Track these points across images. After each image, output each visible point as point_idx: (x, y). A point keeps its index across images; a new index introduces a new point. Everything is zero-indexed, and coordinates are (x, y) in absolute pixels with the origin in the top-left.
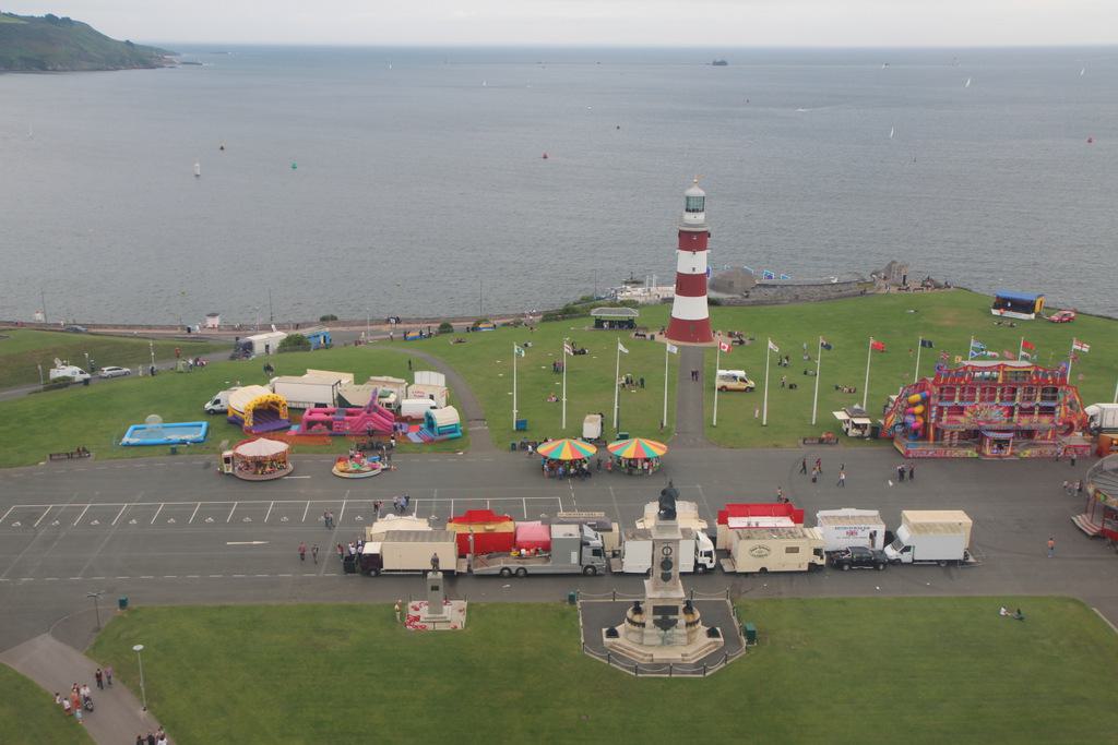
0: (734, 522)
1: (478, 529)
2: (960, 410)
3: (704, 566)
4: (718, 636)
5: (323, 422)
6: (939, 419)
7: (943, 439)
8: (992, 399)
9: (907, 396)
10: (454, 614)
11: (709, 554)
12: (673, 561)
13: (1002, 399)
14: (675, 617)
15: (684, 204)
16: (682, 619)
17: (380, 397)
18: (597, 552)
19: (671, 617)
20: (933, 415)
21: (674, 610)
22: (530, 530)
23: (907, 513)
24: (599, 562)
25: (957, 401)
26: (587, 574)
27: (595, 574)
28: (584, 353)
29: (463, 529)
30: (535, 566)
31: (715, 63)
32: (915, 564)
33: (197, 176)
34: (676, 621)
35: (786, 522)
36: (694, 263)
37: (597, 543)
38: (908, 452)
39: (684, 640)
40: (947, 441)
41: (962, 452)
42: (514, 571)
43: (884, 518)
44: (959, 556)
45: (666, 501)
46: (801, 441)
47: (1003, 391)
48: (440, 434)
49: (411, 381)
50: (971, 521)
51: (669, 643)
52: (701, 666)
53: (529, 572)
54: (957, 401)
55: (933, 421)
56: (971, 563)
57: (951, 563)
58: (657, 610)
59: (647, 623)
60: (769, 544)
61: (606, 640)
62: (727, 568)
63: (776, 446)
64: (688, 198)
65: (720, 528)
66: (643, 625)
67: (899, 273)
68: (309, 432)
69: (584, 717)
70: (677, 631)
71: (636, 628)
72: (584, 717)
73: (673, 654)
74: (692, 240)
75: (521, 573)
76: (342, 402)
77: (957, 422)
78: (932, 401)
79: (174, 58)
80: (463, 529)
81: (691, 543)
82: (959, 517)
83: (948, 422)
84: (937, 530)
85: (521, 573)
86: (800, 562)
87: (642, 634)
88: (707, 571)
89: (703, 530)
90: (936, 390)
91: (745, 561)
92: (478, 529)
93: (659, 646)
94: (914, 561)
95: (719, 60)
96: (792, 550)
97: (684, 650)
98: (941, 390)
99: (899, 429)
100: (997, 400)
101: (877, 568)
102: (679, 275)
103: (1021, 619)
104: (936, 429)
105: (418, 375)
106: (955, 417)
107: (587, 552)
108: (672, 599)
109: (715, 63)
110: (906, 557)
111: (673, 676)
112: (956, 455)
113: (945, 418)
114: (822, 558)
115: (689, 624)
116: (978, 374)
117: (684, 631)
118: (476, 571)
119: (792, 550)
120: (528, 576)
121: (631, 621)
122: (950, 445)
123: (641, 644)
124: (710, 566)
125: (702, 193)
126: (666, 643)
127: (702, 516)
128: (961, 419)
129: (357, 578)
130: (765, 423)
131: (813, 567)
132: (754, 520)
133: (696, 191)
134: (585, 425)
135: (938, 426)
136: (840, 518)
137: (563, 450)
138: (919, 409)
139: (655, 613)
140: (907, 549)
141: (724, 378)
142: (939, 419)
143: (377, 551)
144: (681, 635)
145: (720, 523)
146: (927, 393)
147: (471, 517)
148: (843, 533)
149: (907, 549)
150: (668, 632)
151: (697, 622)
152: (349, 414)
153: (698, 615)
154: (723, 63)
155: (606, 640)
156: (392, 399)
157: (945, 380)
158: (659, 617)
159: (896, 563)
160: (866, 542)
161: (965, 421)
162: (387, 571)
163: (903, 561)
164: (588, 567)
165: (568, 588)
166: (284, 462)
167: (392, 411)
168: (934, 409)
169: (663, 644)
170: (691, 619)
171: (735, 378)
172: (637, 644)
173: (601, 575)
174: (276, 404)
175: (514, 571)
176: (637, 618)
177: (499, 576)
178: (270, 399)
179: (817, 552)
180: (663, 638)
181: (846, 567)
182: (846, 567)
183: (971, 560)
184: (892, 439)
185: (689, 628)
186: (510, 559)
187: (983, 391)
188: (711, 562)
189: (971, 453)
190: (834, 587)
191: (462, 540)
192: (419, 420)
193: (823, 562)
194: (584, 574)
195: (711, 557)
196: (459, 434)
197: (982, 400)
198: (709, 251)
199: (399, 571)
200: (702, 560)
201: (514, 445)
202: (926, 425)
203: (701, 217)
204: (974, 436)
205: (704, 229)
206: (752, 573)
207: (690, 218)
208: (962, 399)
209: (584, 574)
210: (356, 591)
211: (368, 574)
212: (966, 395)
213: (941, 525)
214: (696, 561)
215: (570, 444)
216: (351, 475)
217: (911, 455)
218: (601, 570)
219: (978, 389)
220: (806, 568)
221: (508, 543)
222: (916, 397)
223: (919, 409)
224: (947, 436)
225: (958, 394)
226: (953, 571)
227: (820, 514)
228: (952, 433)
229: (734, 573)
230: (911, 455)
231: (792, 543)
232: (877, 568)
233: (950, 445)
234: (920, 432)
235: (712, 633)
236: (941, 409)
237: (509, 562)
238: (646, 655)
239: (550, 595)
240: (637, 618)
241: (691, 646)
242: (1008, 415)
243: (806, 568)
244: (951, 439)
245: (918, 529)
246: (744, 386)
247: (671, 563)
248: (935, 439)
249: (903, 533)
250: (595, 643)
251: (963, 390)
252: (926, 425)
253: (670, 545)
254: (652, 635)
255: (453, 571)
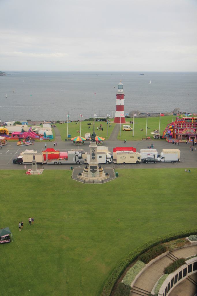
0: (117, 152)
1: (50, 153)
2: (182, 130)
3: (108, 162)
4: (108, 175)
5: (17, 135)
6: (177, 132)
7: (178, 137)
8: (191, 127)
9: (169, 127)
10: (39, 171)
11: (109, 158)
12: (95, 154)
13: (193, 127)
14: (96, 169)
15: (117, 87)
16: (98, 170)
17: (33, 129)
18: (80, 158)
19: (95, 169)
20: (175, 131)
21: (96, 167)
22: (63, 153)
23: (164, 150)
24: (80, 160)
25: (181, 127)
26: (78, 164)
27: (79, 164)
28: (91, 124)
29: (44, 153)
30: (64, 162)
31: (141, 75)
32: (165, 162)
33: (6, 98)
34: (96, 170)
35: (132, 152)
36: (121, 102)
37: (80, 155)
38: (169, 141)
39: (98, 175)
40: (179, 138)
41: (183, 141)
42: (58, 163)
43: (157, 151)
44: (176, 160)
45: (93, 137)
46: (142, 140)
47: (193, 125)
48: (47, 138)
49: (42, 127)
50: (180, 151)
51: (94, 176)
52: (102, 182)
53: (62, 163)
54: (181, 127)
55: (175, 133)
56: (180, 162)
57: (175, 162)
58: (91, 167)
59: (89, 171)
60: (125, 157)
61: (78, 176)
62: (115, 162)
63: (135, 140)
64: (119, 85)
65: (114, 153)
66: (88, 171)
67: (177, 110)
68: (13, 137)
69: (68, 192)
70: (96, 173)
71: (86, 172)
72: (68, 192)
73: (95, 179)
74: (120, 96)
75: (60, 163)
76: (23, 131)
77: (181, 133)
78: (175, 127)
79: (5, 74)
80: (44, 153)
81: (105, 155)
82: (178, 151)
83: (180, 133)
84: (172, 154)
85: (60, 163)
86: (134, 161)
87: (87, 174)
88: (110, 163)
89: (109, 154)
90: (176, 124)
91: (119, 161)
92: (50, 153)
93: (92, 177)
94: (165, 161)
95: (142, 74)
96: (132, 157)
97: (98, 178)
98: (177, 124)
99: (167, 136)
100: (192, 127)
101: (155, 163)
102: (117, 106)
103: (190, 172)
104: (176, 135)
105: (44, 125)
106: (181, 132)
107: (77, 158)
108: (95, 164)
109: (141, 75)
110: (163, 160)
111: (94, 183)
112: (181, 141)
113: (178, 132)
114: (140, 160)
115: (99, 171)
116: (182, 116)
117: (99, 173)
118: (48, 163)
119: (132, 157)
120: (62, 164)
121: (85, 171)
122: (180, 139)
123: (87, 177)
124: (110, 162)
125: (122, 84)
126: (94, 176)
127: (109, 150)
128: (183, 132)
129: (16, 165)
130: (133, 136)
131: (138, 163)
132: (122, 151)
133: (121, 84)
134: (85, 135)
135: (177, 134)
136: (146, 151)
137: (77, 139)
138: (172, 130)
139: (90, 168)
140: (163, 158)
141: (125, 127)
142: (177, 132)
143: (21, 158)
144: (98, 174)
145: (114, 152)
146: (174, 125)
147: (48, 150)
148: (146, 154)
149: (163, 158)
150: (94, 173)
151: (103, 171)
152: (24, 133)
153: (103, 169)
154: (143, 75)
155: (78, 176)
156: (36, 130)
157: (178, 122)
158: (92, 169)
159: (160, 162)
160: (153, 157)
161: (184, 133)
162: (24, 163)
163: (162, 161)
164: (78, 162)
165: (72, 166)
166: (4, 142)
167: (36, 133)
168: (176, 129)
169: (93, 177)
170: (100, 170)
171: (127, 127)
172: (87, 176)
173: (81, 164)
174: (5, 131)
175: (58, 163)
176: (86, 170)
177: (54, 164)
178: (4, 129)
179: (139, 158)
180: (93, 175)
181: (147, 162)
182: (147, 162)
183: (180, 161)
184: (165, 138)
185: (100, 173)
186: (57, 160)
187: (188, 125)
188: (110, 161)
189: (185, 141)
190: (141, 167)
191: (44, 156)
192: (43, 136)
193: (140, 161)
194: (77, 164)
195: (110, 159)
196: (52, 138)
197: (188, 127)
198: (124, 100)
199: (27, 163)
200: (108, 160)
201: (66, 140)
202: (174, 134)
203: (122, 90)
204: (187, 137)
205: (123, 94)
206: (121, 164)
207: (119, 91)
208: (183, 127)
209: (77, 164)
210: (17, 168)
211: (19, 164)
212: (184, 126)
213: (172, 152)
214: (106, 161)
215: (79, 138)
216: (21, 145)
217: (169, 142)
218: (81, 164)
219: (187, 124)
220: (136, 163)
221: (57, 157)
222: (171, 127)
223: (172, 130)
224: (179, 136)
225: (182, 125)
226: (175, 163)
227: (141, 150)
228: (180, 136)
229: (116, 164)
230: (169, 142)
231: (132, 155)
232: (155, 163)
233: (180, 139)
234: (172, 136)
235: (107, 174)
236: (177, 129)
237: (58, 161)
238: (88, 179)
239: (67, 168)
240: (86, 170)
241: (101, 177)
242: (195, 131)
243: (136, 163)
244: (180, 137)
245: (166, 153)
246: (130, 129)
247: (95, 154)
248: (176, 137)
249: (162, 154)
250: (75, 176)
251: (183, 125)
252: (174, 134)
253: (94, 149)
254: (90, 174)
255: (42, 163)
